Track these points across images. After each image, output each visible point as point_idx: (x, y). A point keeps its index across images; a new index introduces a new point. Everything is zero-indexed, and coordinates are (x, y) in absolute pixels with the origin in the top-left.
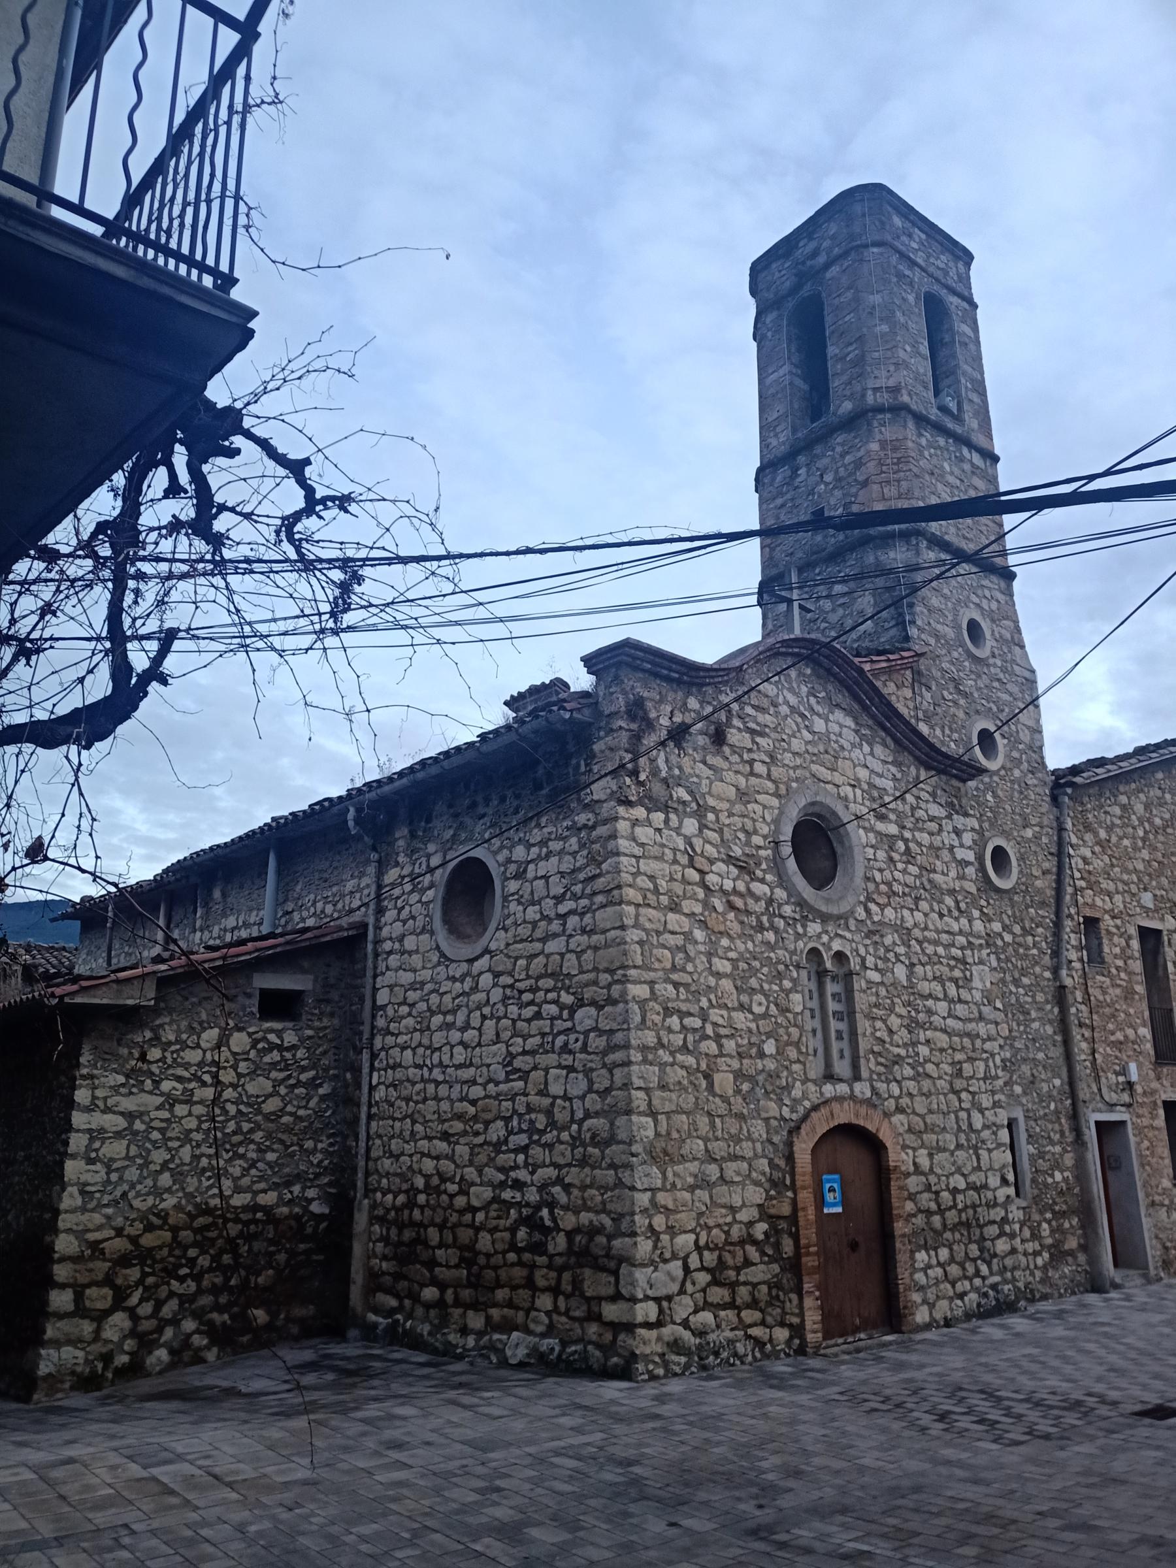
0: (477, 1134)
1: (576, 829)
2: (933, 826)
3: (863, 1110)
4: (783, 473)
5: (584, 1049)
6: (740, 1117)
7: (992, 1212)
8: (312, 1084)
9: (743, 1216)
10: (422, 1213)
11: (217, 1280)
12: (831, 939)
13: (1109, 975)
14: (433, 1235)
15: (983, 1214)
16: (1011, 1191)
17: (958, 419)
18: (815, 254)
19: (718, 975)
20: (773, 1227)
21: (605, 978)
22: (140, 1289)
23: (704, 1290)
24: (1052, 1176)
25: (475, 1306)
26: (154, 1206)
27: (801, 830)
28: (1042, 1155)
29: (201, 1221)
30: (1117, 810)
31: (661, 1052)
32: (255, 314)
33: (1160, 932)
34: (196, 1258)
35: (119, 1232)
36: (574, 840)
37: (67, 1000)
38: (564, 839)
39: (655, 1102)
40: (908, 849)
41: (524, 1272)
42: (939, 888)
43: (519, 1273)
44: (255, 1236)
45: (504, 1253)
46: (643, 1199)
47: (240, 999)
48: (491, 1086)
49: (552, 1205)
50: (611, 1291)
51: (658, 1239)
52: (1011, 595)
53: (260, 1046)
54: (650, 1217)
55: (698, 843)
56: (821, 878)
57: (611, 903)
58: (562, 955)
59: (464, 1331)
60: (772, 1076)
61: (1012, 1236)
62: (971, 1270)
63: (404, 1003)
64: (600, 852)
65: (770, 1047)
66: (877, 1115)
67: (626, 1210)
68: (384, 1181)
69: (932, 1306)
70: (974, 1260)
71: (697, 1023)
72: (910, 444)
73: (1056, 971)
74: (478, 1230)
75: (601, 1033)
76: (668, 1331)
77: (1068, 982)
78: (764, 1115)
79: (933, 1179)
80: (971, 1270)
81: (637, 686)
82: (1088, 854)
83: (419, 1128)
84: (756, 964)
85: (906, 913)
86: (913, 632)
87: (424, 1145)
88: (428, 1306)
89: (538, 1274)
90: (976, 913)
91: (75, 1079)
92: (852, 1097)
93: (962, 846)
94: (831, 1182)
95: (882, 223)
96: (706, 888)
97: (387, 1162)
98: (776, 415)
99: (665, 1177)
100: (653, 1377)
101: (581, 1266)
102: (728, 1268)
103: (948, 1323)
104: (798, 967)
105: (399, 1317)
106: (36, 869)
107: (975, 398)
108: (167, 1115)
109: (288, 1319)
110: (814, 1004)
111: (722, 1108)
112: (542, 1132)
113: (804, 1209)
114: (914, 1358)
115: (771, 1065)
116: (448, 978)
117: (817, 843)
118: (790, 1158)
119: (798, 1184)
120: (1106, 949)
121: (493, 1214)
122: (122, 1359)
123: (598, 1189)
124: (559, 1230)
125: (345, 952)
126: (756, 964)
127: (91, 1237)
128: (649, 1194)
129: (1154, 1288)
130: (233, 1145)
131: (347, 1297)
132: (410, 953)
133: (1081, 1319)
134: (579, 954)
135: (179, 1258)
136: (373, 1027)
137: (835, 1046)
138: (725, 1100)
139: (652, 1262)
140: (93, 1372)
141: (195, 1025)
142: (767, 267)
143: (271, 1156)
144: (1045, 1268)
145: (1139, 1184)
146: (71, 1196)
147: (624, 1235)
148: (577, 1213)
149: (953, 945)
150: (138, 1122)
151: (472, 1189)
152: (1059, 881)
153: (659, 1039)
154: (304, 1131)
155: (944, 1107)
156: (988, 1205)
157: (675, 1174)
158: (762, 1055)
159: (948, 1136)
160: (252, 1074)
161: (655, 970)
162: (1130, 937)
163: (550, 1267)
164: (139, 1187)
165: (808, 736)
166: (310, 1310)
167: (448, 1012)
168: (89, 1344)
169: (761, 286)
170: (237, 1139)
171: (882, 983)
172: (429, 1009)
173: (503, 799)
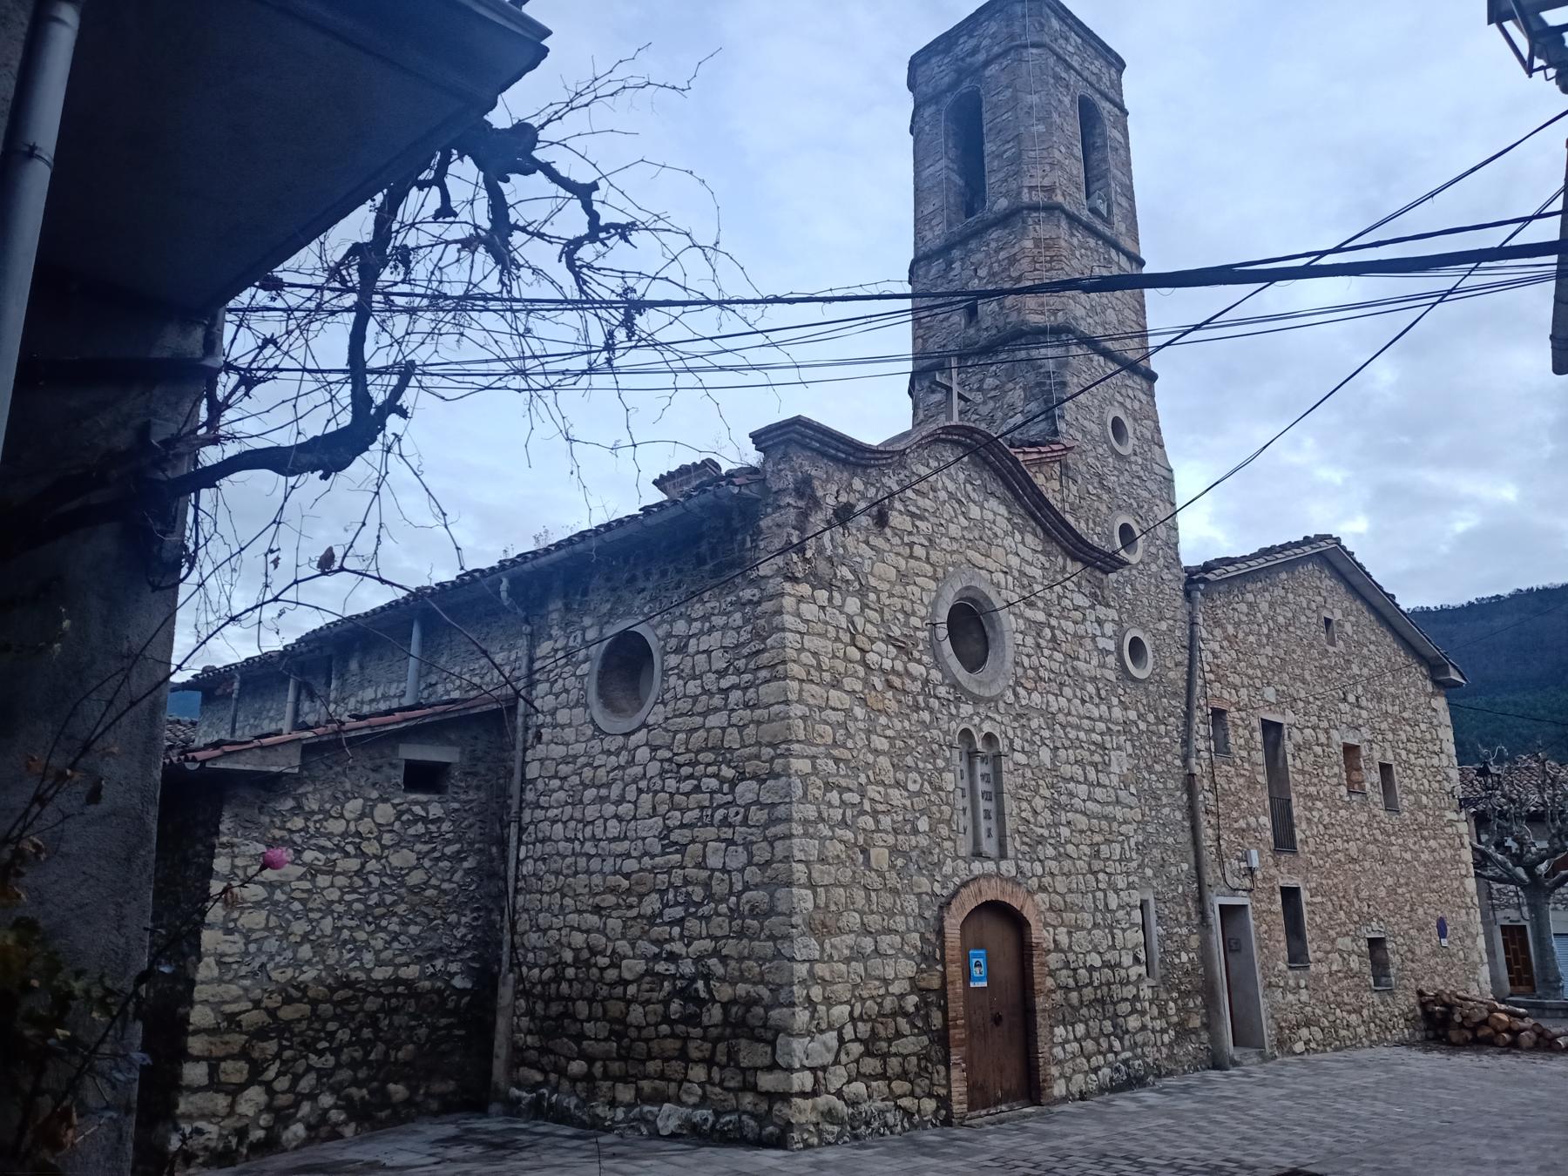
0: (631, 907)
1: (741, 604)
2: (1077, 615)
3: (1009, 888)
4: (937, 266)
5: (745, 822)
6: (894, 891)
7: (1125, 990)
8: (457, 858)
9: (896, 988)
10: (571, 986)
11: (356, 1055)
12: (982, 721)
13: (1234, 765)
14: (582, 1008)
15: (1117, 991)
16: (1143, 970)
17: (1107, 221)
18: (975, 51)
19: (876, 752)
20: (923, 999)
21: (767, 752)
22: (277, 1064)
23: (857, 1061)
24: (1179, 957)
25: (624, 1079)
26: (294, 978)
27: (956, 611)
28: (1169, 936)
29: (340, 995)
30: (1244, 608)
31: (821, 826)
32: (549, 33)
33: (1280, 725)
35: (257, 1004)
36: (738, 615)
37: (208, 765)
38: (728, 614)
39: (815, 875)
40: (1054, 635)
41: (678, 1044)
42: (1083, 676)
43: (672, 1045)
44: (396, 1010)
45: (657, 1025)
46: (802, 970)
47: (386, 769)
48: (646, 859)
49: (707, 977)
50: (767, 1061)
51: (815, 1010)
52: (1153, 396)
53: (404, 818)
54: (808, 988)
55: (859, 621)
56: (974, 663)
57: (776, 678)
58: (723, 729)
59: (613, 1104)
60: (926, 852)
61: (1143, 1013)
62: (1105, 1045)
63: (555, 776)
64: (764, 628)
65: (923, 824)
66: (1021, 893)
67: (784, 980)
68: (531, 955)
69: (1069, 1079)
70: (1108, 1036)
71: (856, 798)
72: (1063, 244)
73: (1185, 759)
74: (629, 1002)
75: (762, 806)
76: (823, 1101)
77: (1197, 770)
78: (916, 890)
79: (1071, 957)
80: (1105, 1045)
81: (804, 463)
82: (1218, 649)
83: (568, 901)
84: (912, 742)
85: (1051, 698)
86: (1062, 426)
87: (573, 919)
88: (574, 1080)
89: (692, 1045)
90: (1115, 701)
91: (214, 847)
92: (999, 875)
93: (1103, 635)
94: (978, 956)
95: (1042, 25)
96: (867, 666)
97: (534, 936)
98: (931, 208)
99: (823, 950)
100: (808, 1146)
101: (737, 1037)
102: (880, 1039)
103: (1083, 1096)
104: (951, 747)
105: (544, 1091)
106: (325, 581)
107: (1125, 203)
108: (308, 885)
109: (428, 1095)
110: (965, 784)
111: (876, 881)
112: (699, 905)
113: (953, 983)
114: (1055, 1128)
115: (924, 841)
116: (603, 752)
117: (970, 626)
118: (940, 933)
119: (948, 958)
120: (1232, 741)
121: (645, 986)
122: (257, 1134)
123: (756, 960)
124: (714, 1001)
125: (494, 725)
126: (912, 742)
127: (228, 1008)
128: (807, 965)
129: (1270, 1065)
130: (375, 918)
131: (489, 1073)
132: (563, 727)
133: (1208, 1093)
134: (741, 728)
135: (318, 1031)
136: (522, 801)
137: (984, 825)
138: (881, 874)
139: (809, 1033)
140: (227, 1147)
141: (339, 795)
142: (927, 61)
143: (414, 930)
144: (1170, 1045)
145: (1257, 966)
146: (208, 966)
147: (781, 1005)
148: (733, 984)
149: (1093, 731)
150: (278, 892)
151: (624, 962)
152: (1190, 673)
153: (820, 813)
154: (448, 905)
155: (1082, 887)
156: (1121, 983)
157: (833, 946)
158: (915, 832)
159: (1086, 915)
160: (397, 846)
161: (817, 745)
162: (1254, 730)
163: (704, 1039)
164: (278, 959)
165: (965, 523)
166: (451, 1085)
167: (602, 786)
168: (223, 1118)
169: (920, 80)
170: (379, 911)
171: (1028, 765)
172: (582, 783)
173: (664, 574)
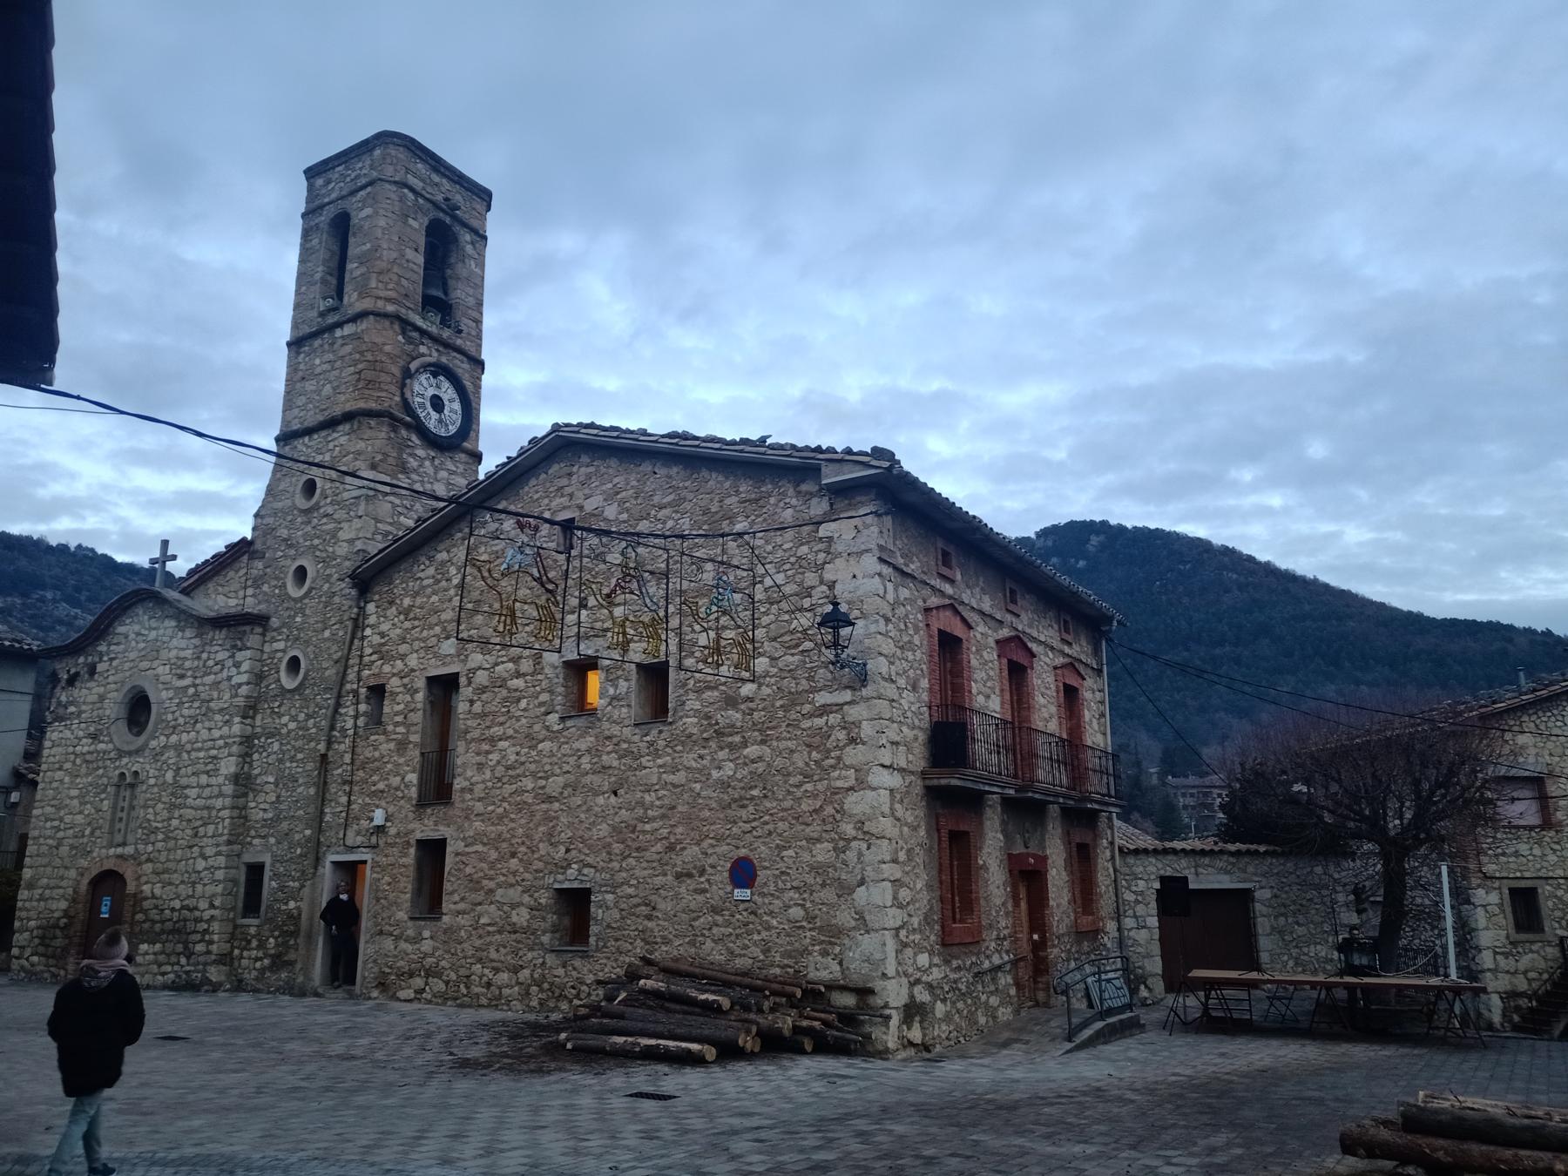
9: (56, 915)
13: (385, 733)
15: (190, 926)
34: (996, 1009)
144: (263, 970)
